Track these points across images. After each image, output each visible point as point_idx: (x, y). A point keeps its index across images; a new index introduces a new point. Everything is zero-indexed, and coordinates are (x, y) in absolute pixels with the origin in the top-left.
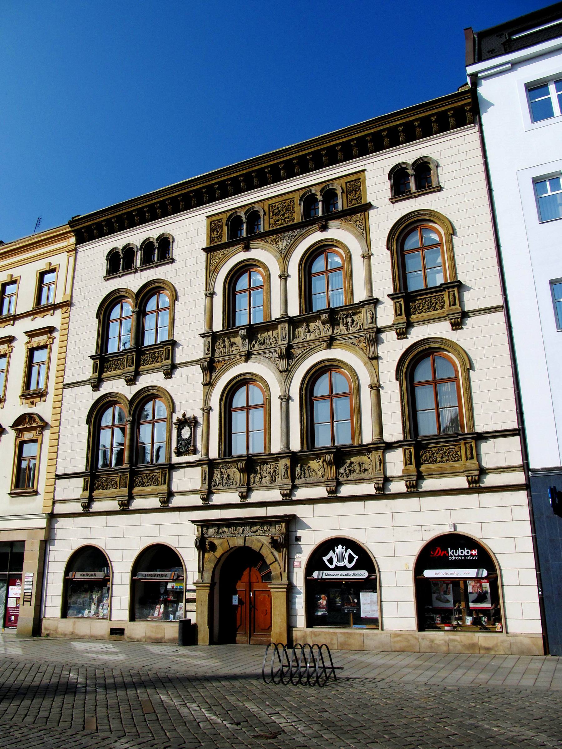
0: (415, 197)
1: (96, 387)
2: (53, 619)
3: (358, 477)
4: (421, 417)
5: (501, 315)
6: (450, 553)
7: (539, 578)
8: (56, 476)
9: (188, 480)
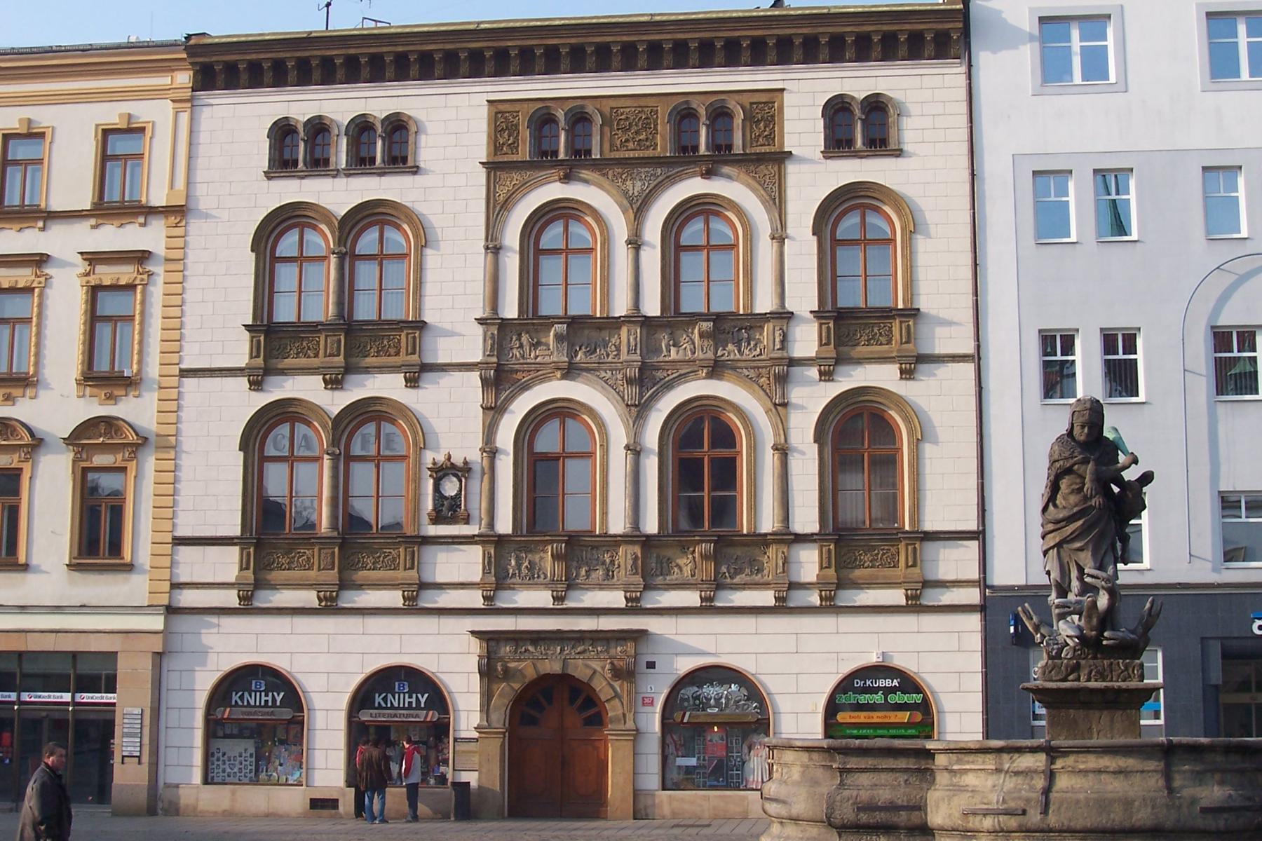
0: (861, 157)
5: (969, 368)
9: (460, 565)
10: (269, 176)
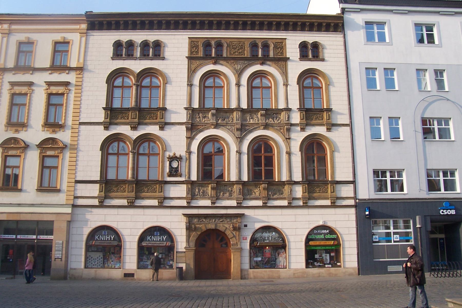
1: (106, 128)
3: (278, 197)
5: (348, 129)
8: (76, 181)
9: (180, 191)
10: (113, 59)
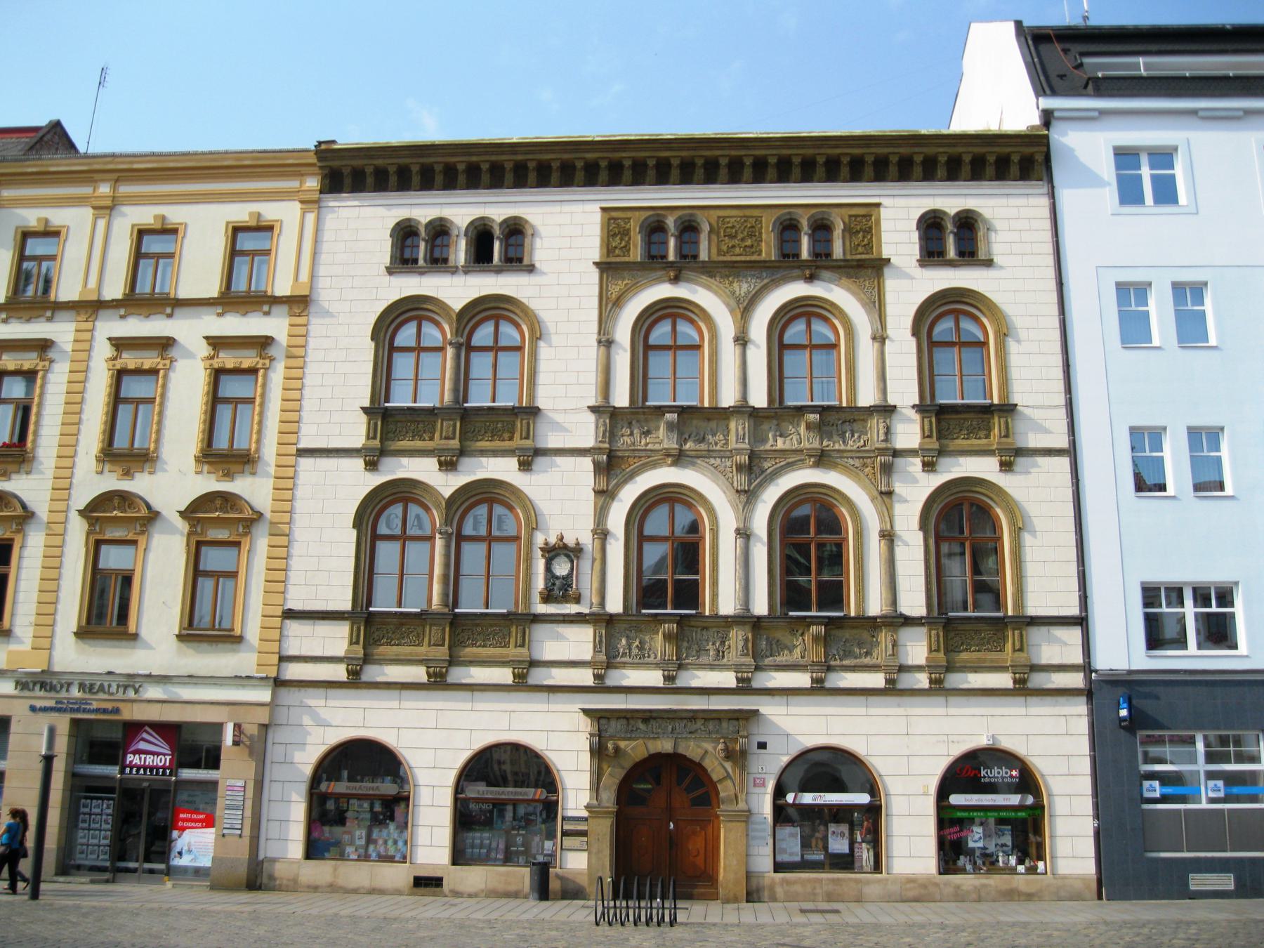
1: (372, 465)
2: (292, 862)
3: (858, 661)
4: (465, 584)
5: (1065, 462)
6: (983, 773)
7: (1096, 806)
10: (390, 271)
